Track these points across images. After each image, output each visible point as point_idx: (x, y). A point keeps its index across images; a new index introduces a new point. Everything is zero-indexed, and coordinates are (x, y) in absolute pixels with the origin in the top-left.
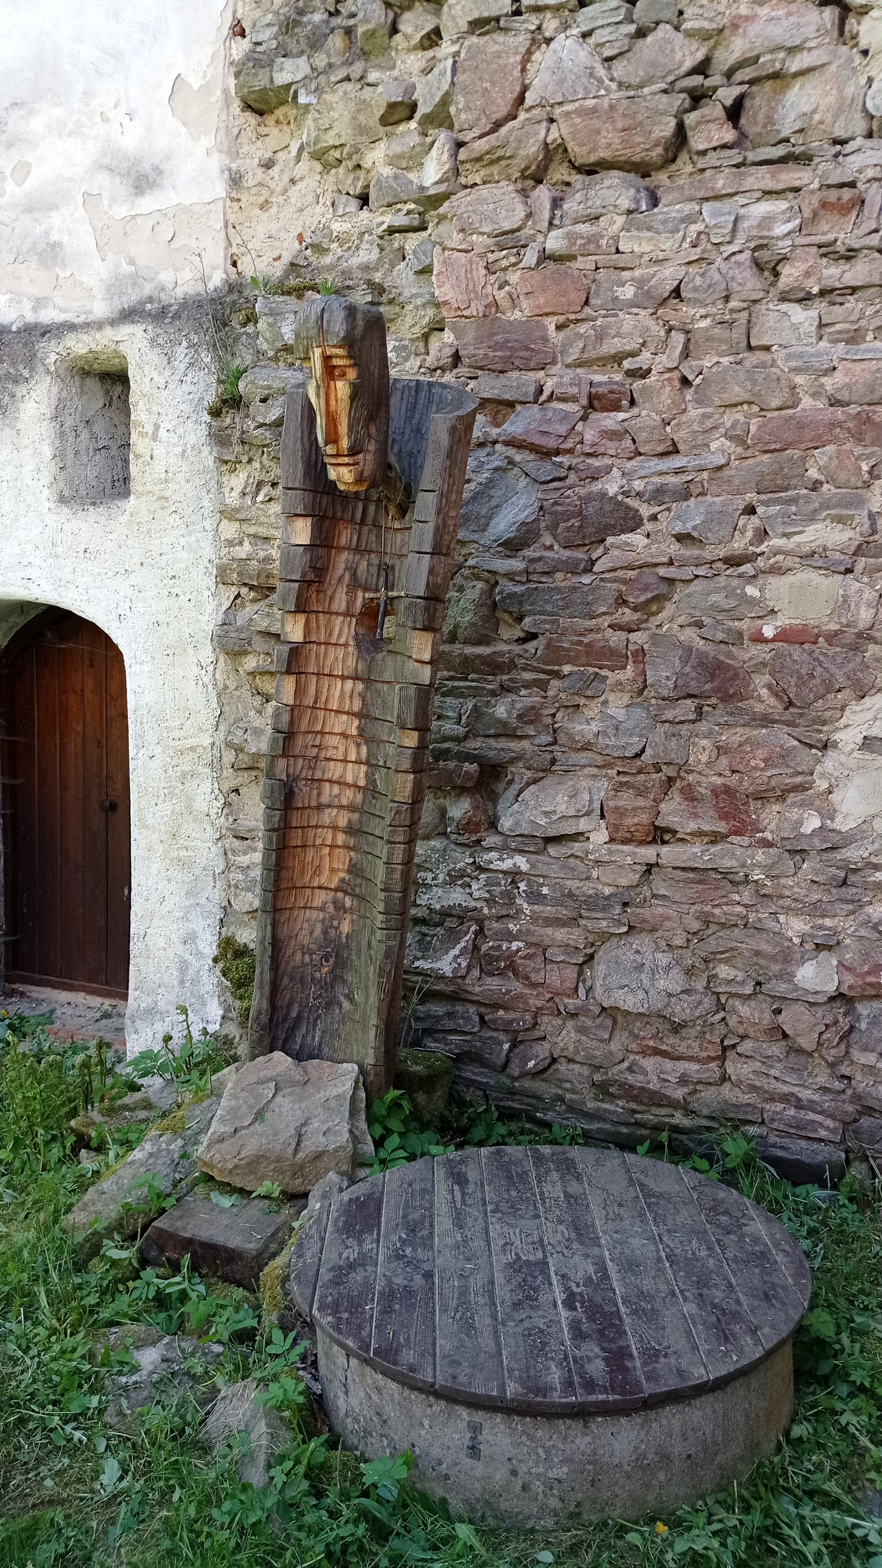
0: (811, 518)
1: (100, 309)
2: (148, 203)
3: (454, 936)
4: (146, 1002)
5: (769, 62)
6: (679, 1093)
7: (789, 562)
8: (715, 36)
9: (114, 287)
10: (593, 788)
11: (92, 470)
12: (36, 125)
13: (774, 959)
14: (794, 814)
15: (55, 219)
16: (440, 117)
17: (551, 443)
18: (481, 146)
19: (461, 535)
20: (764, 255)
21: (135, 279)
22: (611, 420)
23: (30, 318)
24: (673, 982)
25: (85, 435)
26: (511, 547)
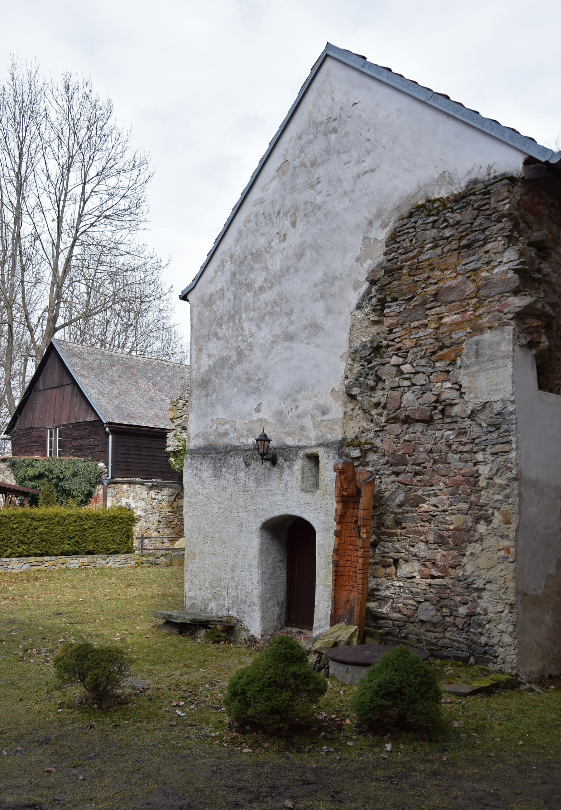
0: (460, 502)
1: (313, 443)
2: (326, 417)
3: (387, 603)
4: (318, 624)
5: (448, 402)
6: (435, 641)
7: (456, 512)
8: (438, 395)
9: (317, 438)
10: (417, 566)
11: (310, 482)
12: (300, 397)
13: (454, 606)
14: (458, 571)
15: (304, 420)
16: (384, 407)
17: (407, 483)
18: (392, 415)
19: (388, 503)
20: (448, 443)
21: (322, 437)
22: (419, 478)
23: (297, 444)
24: (433, 612)
25: (310, 472)
26: (400, 506)
